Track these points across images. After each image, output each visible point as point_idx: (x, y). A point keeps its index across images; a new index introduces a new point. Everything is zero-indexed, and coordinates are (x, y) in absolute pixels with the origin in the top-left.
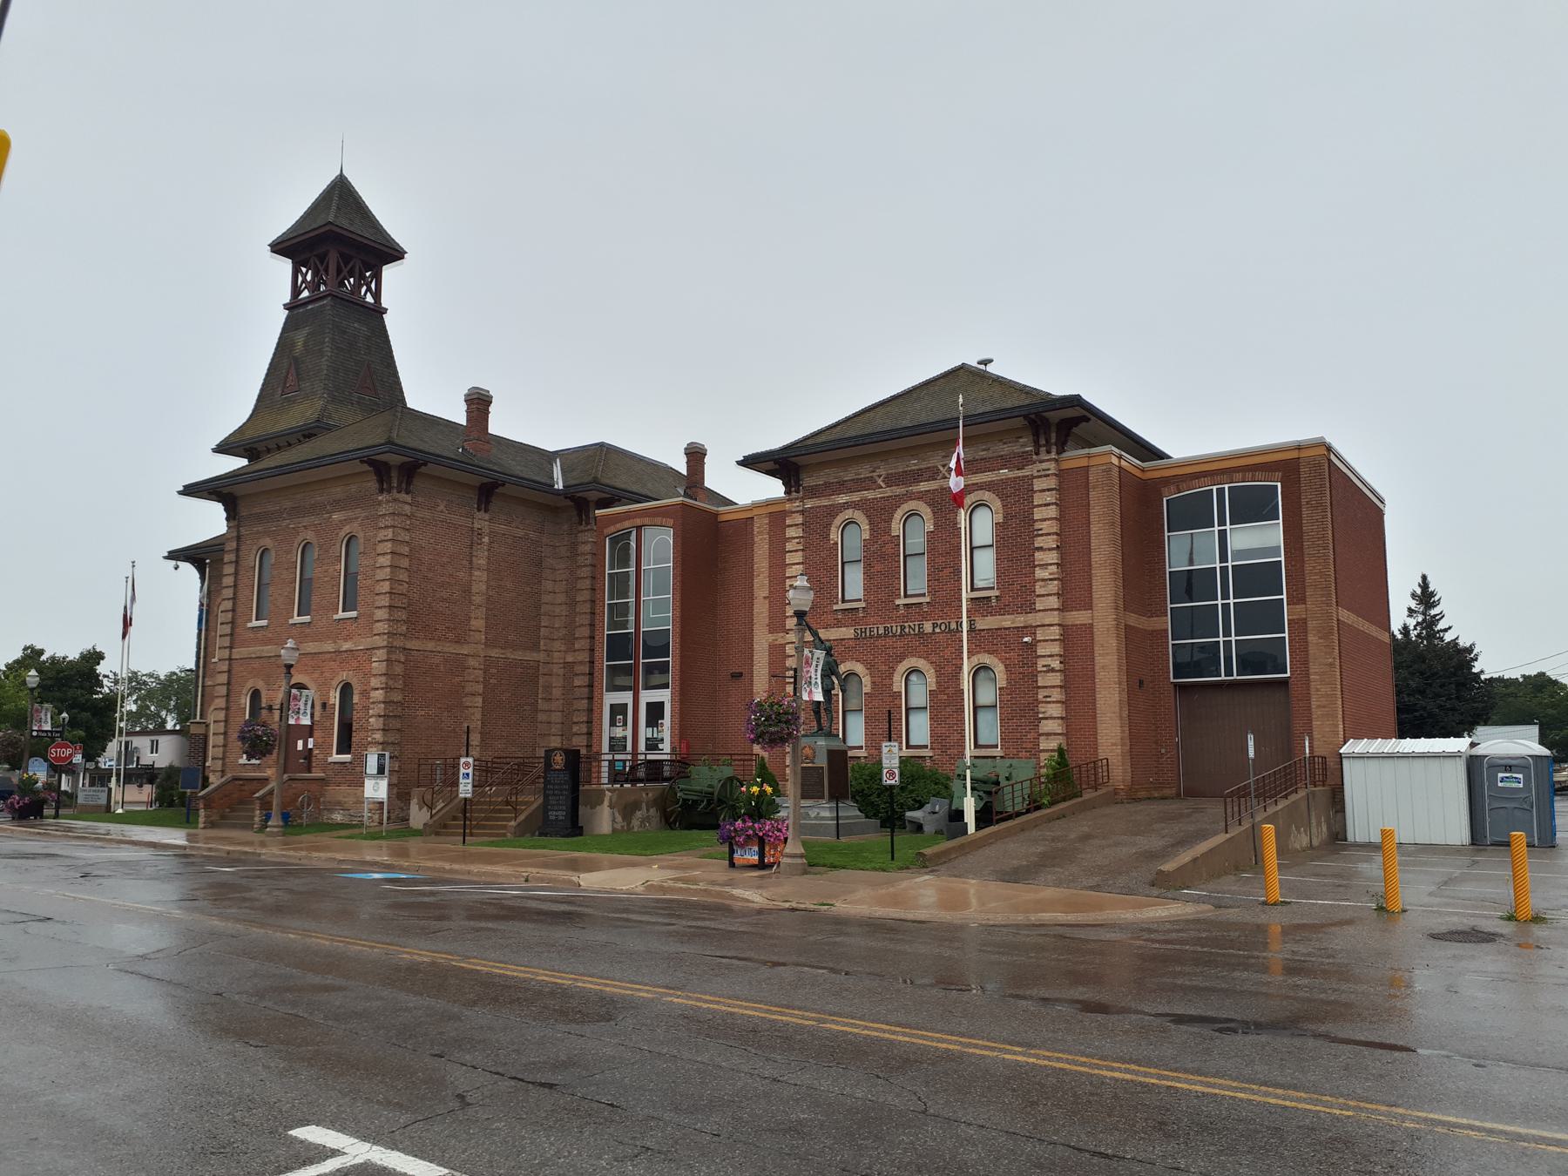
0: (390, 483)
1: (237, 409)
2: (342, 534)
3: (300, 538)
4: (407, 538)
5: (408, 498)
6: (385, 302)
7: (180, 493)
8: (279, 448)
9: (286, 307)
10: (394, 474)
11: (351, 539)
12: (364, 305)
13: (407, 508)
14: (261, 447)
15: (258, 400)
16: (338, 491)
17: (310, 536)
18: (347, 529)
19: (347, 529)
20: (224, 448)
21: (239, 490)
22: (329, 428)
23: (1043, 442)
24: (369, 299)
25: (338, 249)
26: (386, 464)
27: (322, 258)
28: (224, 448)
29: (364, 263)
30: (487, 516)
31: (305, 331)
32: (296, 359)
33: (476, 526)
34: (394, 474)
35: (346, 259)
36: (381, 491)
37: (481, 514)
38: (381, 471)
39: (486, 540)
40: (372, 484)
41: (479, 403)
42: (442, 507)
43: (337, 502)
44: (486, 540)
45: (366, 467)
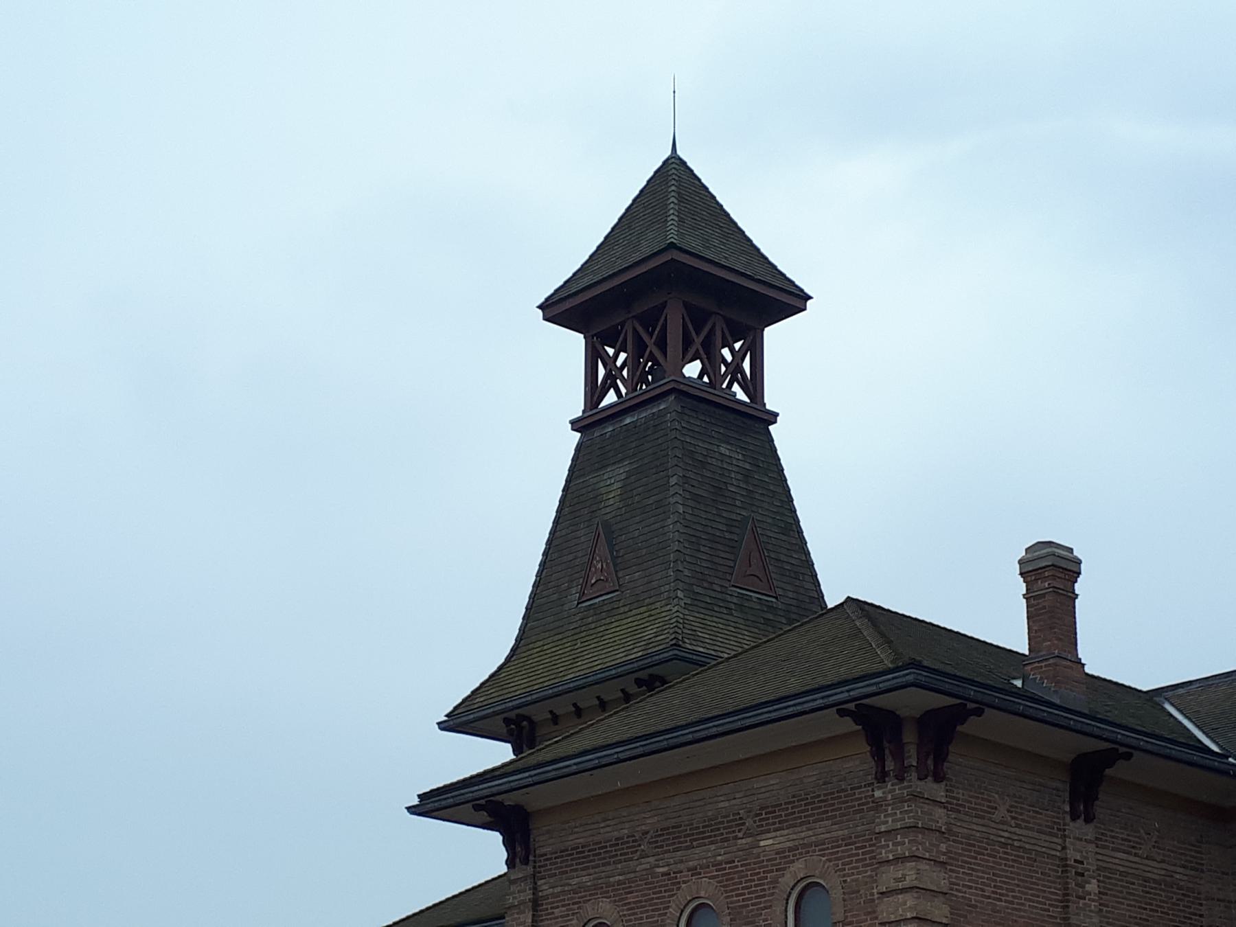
0: (899, 755)
2: (787, 880)
3: (787, 880)
4: (944, 885)
5: (938, 791)
6: (771, 401)
7: (412, 810)
8: (603, 705)
9: (576, 425)
10: (909, 737)
11: (808, 889)
12: (735, 409)
14: (540, 714)
17: (706, 889)
18: (798, 868)
19: (798, 868)
21: (534, 799)
22: (698, 663)
24: (741, 396)
25: (675, 298)
27: (651, 319)
28: (462, 720)
29: (729, 322)
30: (1089, 831)
31: (621, 471)
33: (1072, 854)
34: (909, 737)
35: (697, 318)
36: (882, 777)
37: (1078, 828)
38: (878, 727)
39: (1092, 886)
40: (857, 761)
41: (1051, 577)
42: (1001, 813)
44: (1092, 886)
45: (848, 725)
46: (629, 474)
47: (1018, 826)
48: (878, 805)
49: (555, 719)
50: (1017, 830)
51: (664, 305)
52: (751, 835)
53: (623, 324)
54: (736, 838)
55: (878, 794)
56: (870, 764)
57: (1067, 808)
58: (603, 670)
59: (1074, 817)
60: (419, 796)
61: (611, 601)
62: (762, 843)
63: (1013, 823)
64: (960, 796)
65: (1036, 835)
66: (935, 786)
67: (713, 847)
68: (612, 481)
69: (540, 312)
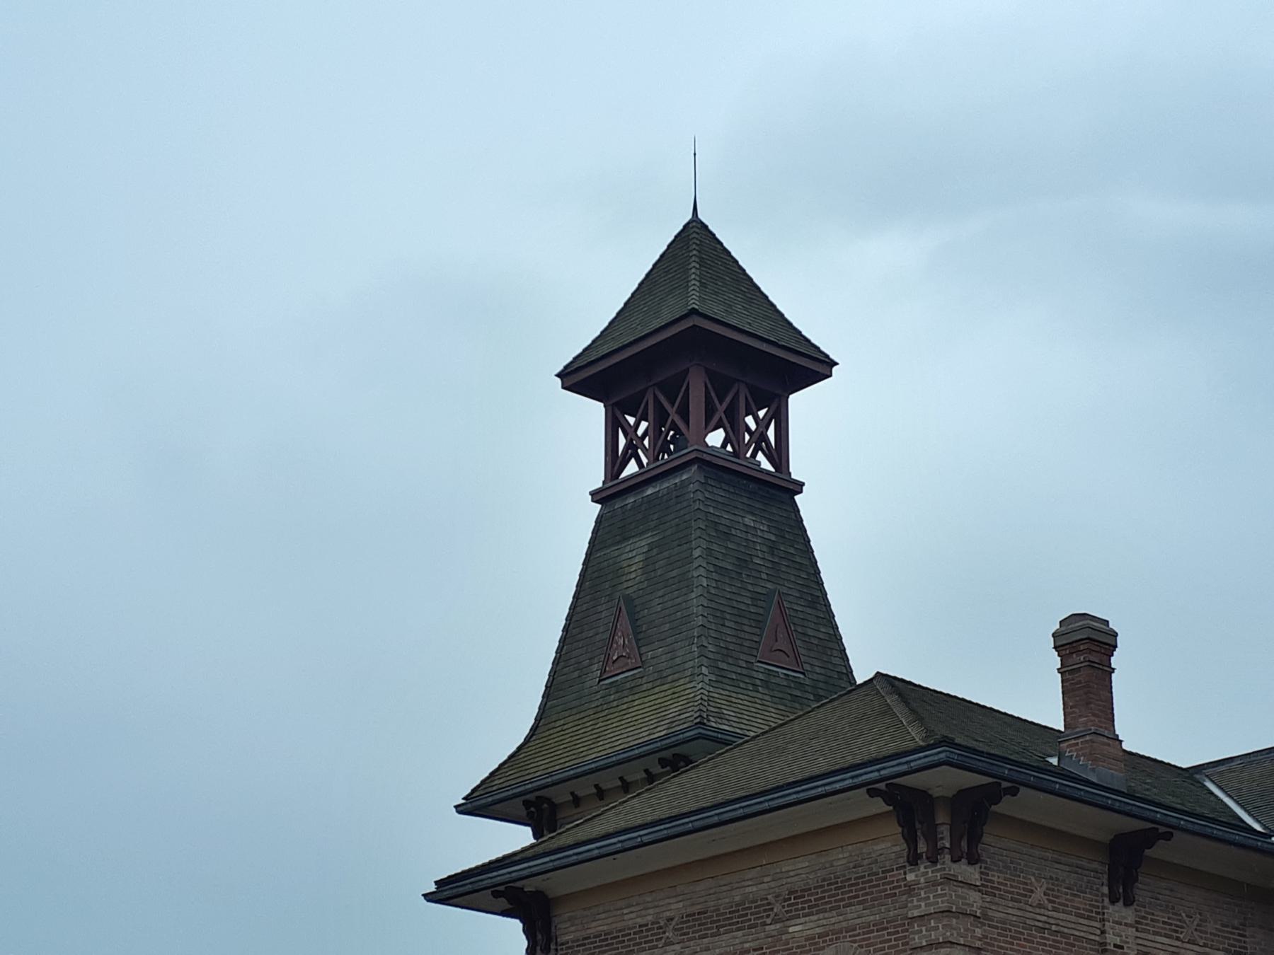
0: (932, 838)
1: (500, 715)
8: (626, 787)
9: (596, 496)
13: (974, 896)
14: (561, 795)
15: (547, 695)
16: (799, 869)
20: (479, 803)
22: (723, 742)
23: (922, 847)
25: (697, 364)
26: (923, 796)
27: (674, 388)
28: (479, 803)
30: (1129, 915)
31: (643, 543)
32: (629, 600)
33: (1111, 939)
34: (942, 818)
35: (719, 385)
36: (914, 859)
37: (1117, 911)
40: (888, 844)
42: (1039, 895)
43: (796, 893)
45: (879, 806)
46: (651, 547)
47: (1055, 910)
48: (910, 889)
49: (577, 801)
50: (1054, 914)
51: (687, 371)
52: (780, 921)
53: (643, 393)
54: (765, 924)
55: (911, 877)
56: (902, 847)
57: (1105, 890)
58: (625, 750)
59: (1113, 902)
60: (436, 883)
61: (634, 678)
62: (791, 930)
63: (1050, 906)
64: (995, 879)
65: (1073, 918)
66: (970, 869)
67: (740, 933)
68: (634, 553)
69: (559, 380)
